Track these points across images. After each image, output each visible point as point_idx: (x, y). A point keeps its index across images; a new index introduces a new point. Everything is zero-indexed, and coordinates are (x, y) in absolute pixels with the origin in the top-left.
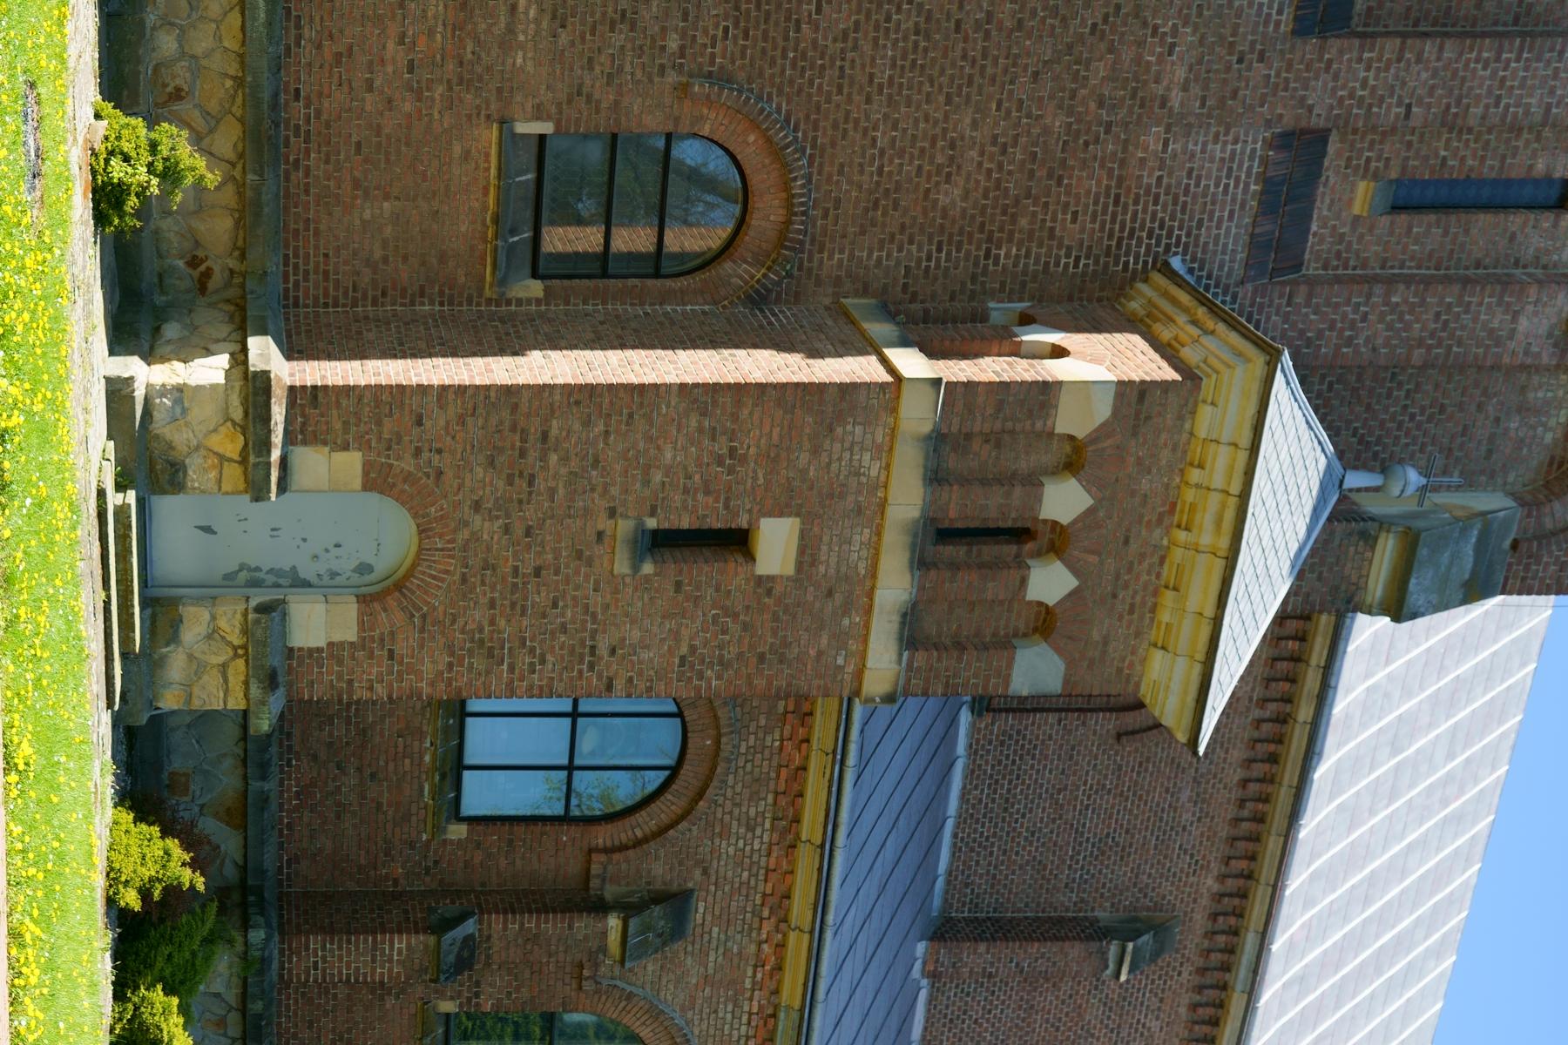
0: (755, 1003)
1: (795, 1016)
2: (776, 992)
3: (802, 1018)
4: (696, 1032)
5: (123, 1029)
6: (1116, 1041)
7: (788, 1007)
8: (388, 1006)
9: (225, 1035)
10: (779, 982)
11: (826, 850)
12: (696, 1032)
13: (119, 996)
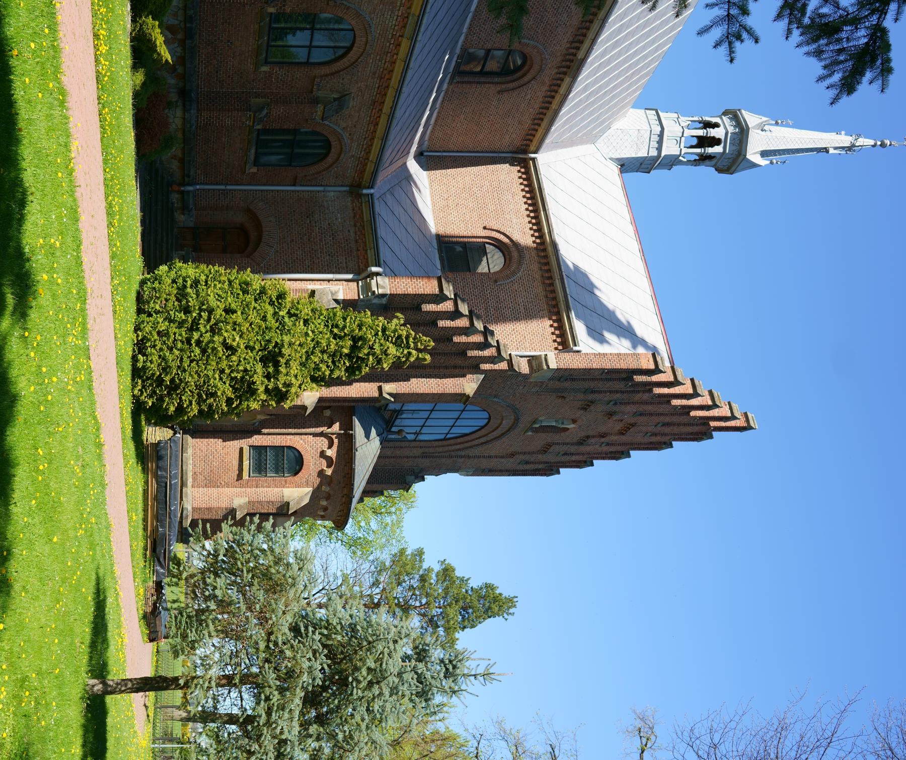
0: (400, 12)
1: (416, 18)
2: (410, 8)
3: (418, 19)
4: (374, 22)
5: (136, 34)
6: (229, 758)
7: (414, 15)
8: (246, 9)
9: (177, 20)
10: (391, 77)
11: (399, 92)
12: (374, 22)
13: (134, 20)
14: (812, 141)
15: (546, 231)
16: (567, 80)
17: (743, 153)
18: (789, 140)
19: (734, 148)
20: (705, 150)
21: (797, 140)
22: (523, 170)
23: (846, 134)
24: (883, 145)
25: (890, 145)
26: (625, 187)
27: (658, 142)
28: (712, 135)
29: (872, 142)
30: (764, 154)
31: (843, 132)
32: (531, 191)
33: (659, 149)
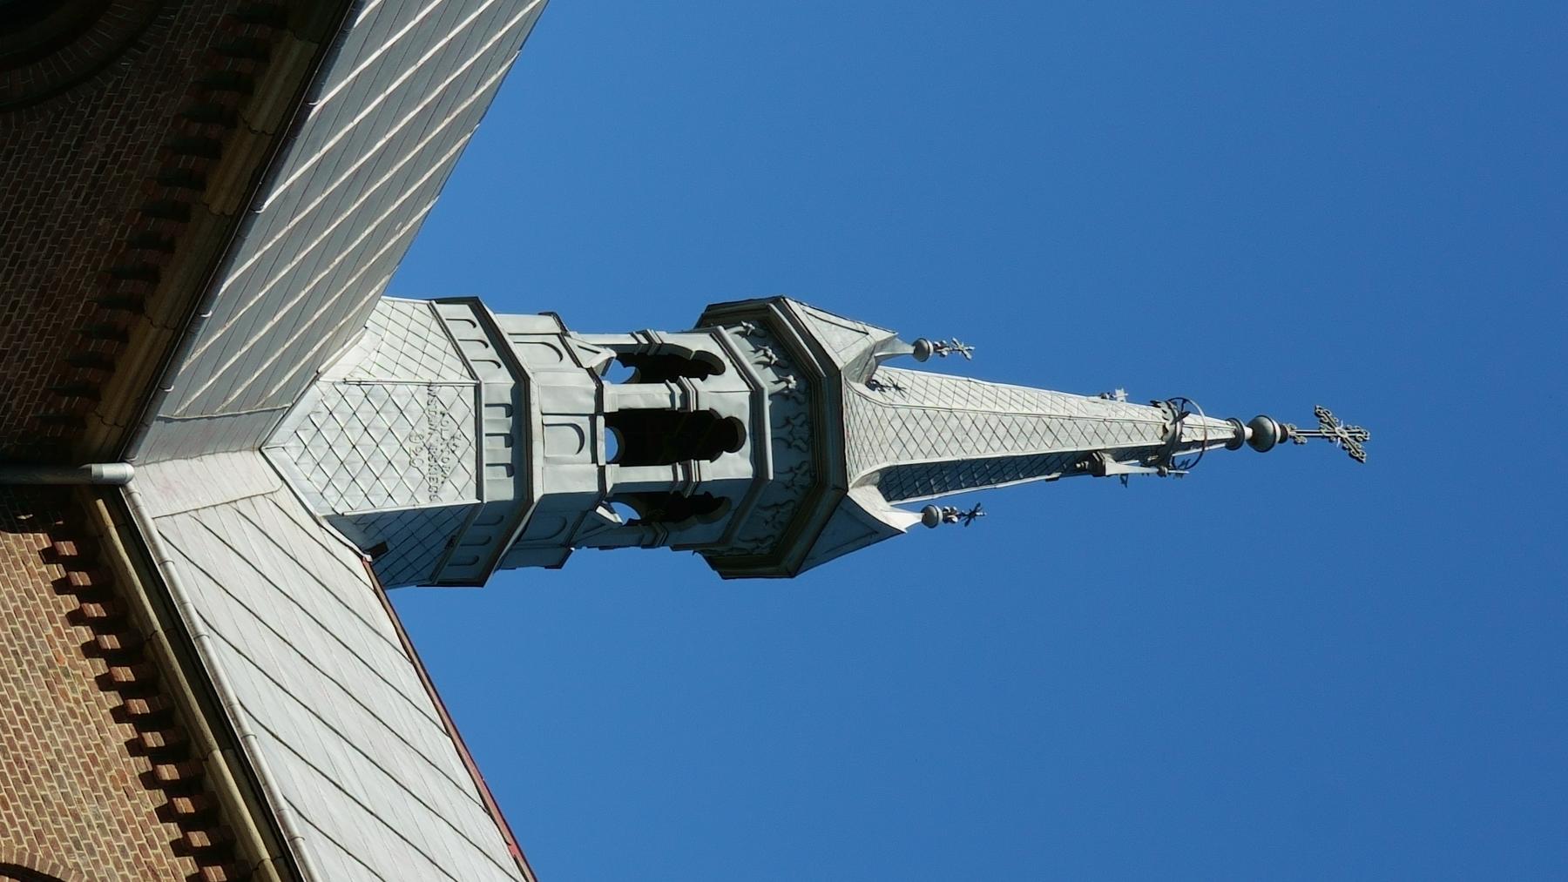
14: (1041, 428)
15: (265, 855)
16: (296, 51)
17: (833, 479)
18: (967, 423)
19: (794, 459)
20: (687, 472)
21: (1007, 421)
22: (67, 548)
23: (1129, 400)
24: (1262, 441)
25: (1284, 437)
26: (1117, 474)
27: (510, 440)
28: (704, 406)
29: (1225, 431)
30: (895, 483)
31: (1120, 394)
32: (136, 650)
33: (521, 469)
